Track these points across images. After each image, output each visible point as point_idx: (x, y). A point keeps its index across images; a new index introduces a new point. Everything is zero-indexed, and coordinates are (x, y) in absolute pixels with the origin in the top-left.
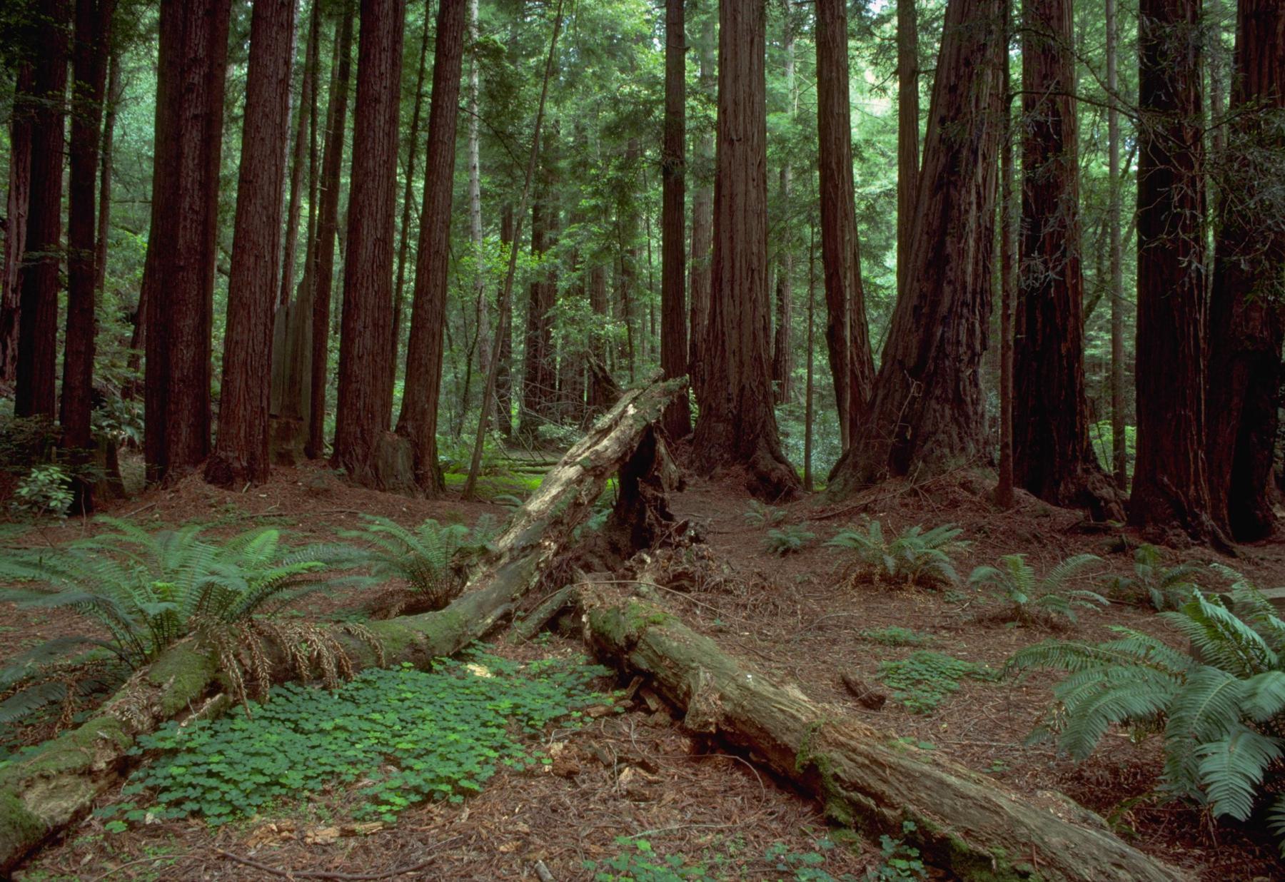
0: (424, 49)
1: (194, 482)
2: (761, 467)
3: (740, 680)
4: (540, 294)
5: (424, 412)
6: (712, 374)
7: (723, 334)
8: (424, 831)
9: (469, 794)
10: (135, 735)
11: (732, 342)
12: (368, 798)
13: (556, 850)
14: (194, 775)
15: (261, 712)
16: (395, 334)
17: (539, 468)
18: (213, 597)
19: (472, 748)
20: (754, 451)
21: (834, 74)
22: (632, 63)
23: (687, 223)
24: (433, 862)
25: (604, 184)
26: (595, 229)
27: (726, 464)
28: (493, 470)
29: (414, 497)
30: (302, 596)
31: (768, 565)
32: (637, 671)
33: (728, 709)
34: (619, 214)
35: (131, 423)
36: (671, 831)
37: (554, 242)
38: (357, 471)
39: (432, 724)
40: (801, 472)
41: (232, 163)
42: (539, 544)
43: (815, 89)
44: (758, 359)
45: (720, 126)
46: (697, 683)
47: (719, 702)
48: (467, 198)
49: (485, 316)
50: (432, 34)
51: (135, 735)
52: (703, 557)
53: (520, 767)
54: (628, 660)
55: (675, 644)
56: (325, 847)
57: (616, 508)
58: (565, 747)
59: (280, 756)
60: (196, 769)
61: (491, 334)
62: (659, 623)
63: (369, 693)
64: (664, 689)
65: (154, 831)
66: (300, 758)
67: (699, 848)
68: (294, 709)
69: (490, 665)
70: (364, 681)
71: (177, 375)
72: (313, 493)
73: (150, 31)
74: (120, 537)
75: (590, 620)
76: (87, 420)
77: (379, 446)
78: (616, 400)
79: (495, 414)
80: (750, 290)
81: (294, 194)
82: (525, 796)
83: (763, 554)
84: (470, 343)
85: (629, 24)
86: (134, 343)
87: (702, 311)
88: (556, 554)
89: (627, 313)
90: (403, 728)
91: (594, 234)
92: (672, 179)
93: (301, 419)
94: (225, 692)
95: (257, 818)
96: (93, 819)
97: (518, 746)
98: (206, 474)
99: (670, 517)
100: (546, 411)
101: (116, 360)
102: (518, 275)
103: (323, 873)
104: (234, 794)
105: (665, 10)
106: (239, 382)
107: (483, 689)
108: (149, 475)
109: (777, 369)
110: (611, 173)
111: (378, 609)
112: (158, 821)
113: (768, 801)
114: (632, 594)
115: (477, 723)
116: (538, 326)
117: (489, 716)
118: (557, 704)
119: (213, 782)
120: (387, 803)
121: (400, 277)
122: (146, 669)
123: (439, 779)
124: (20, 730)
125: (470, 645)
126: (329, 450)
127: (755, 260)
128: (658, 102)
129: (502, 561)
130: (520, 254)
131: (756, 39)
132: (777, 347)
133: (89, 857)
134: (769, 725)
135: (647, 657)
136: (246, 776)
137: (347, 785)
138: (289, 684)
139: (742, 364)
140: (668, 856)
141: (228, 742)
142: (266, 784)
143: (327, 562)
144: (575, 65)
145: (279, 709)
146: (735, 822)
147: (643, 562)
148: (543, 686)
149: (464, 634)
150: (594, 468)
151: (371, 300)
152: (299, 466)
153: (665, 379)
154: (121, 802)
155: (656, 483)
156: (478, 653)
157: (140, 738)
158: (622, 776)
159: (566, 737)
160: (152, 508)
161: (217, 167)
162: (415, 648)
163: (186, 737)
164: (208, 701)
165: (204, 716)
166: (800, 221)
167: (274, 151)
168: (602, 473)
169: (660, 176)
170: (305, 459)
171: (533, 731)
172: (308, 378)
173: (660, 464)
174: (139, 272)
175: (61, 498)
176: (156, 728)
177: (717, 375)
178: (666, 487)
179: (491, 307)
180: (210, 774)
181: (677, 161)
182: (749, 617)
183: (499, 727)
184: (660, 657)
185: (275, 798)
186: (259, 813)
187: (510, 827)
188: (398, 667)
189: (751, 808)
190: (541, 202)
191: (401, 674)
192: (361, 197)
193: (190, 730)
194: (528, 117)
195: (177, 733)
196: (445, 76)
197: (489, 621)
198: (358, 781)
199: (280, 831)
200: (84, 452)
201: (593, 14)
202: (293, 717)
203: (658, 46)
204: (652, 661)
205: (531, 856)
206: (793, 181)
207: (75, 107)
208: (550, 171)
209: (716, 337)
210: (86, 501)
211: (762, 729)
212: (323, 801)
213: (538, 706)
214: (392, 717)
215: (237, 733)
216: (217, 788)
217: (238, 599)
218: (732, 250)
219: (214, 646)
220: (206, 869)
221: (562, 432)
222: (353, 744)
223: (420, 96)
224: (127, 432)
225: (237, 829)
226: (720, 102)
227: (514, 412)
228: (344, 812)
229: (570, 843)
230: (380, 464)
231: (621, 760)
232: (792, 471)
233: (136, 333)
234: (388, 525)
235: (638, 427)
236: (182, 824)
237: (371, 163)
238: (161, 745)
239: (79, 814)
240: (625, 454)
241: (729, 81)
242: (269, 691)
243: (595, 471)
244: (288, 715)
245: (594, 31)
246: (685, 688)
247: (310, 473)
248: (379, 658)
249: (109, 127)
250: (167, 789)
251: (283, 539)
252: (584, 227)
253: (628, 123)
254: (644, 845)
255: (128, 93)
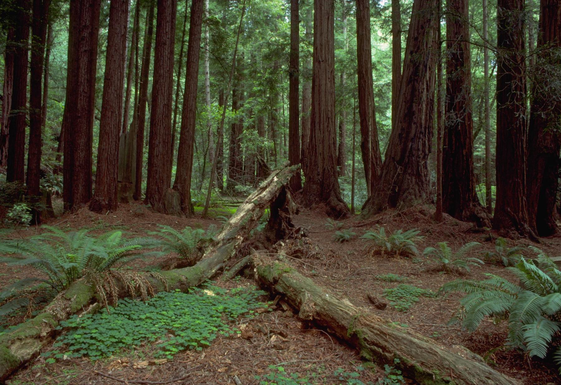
0: (185, 21)
1: (85, 210)
2: (332, 204)
3: (323, 297)
4: (236, 128)
5: (185, 180)
6: (311, 163)
7: (316, 146)
8: (185, 363)
9: (205, 347)
10: (59, 321)
11: (320, 149)
12: (160, 348)
13: (243, 371)
14: (85, 338)
15: (114, 311)
16: (172, 146)
17: (235, 204)
18: (93, 261)
19: (206, 327)
20: (329, 197)
21: (364, 32)
22: (276, 27)
23: (300, 97)
24: (189, 376)
25: (264, 80)
26: (260, 100)
27: (317, 203)
28: (215, 205)
29: (181, 217)
30: (132, 260)
31: (335, 247)
32: (278, 293)
33: (318, 309)
34: (270, 93)
35: (57, 185)
36: (293, 363)
37: (242, 105)
38: (156, 205)
39: (189, 316)
40: (350, 206)
41: (101, 71)
42: (235, 238)
43: (356, 39)
44: (331, 157)
45: (315, 55)
46: (304, 298)
47: (314, 307)
48: (204, 86)
49: (212, 138)
50: (189, 15)
51: (59, 321)
52: (307, 243)
53: (227, 335)
54: (274, 288)
55: (295, 281)
56: (142, 370)
57: (269, 222)
58: (247, 326)
59: (122, 330)
60: (85, 336)
61: (214, 146)
62: (288, 272)
63: (161, 302)
64: (290, 301)
65: (67, 363)
66: (131, 331)
67: (305, 370)
68: (129, 309)
69: (214, 290)
70: (159, 297)
71: (77, 163)
72: (137, 215)
73: (65, 14)
74: (52, 234)
75: (258, 271)
76: (38, 183)
77: (165, 195)
78: (269, 174)
79: (216, 181)
80: (328, 126)
81: (128, 85)
82: (229, 347)
83: (333, 242)
84: (205, 150)
85: (275, 10)
86: (58, 150)
87: (307, 136)
88: (243, 242)
89: (274, 137)
90: (176, 318)
91: (259, 102)
92: (293, 78)
93: (131, 183)
94: (98, 302)
95: (112, 357)
96: (41, 357)
97: (226, 326)
98: (90, 207)
99: (292, 226)
100: (238, 180)
101: (51, 157)
102: (226, 120)
103: (141, 381)
104: (102, 347)
105: (290, 5)
106: (104, 167)
107: (211, 301)
108: (65, 207)
109: (339, 161)
110: (267, 75)
111: (165, 266)
112: (69, 358)
113: (335, 350)
114: (276, 259)
115: (208, 316)
116: (235, 142)
117: (213, 313)
118: (243, 307)
119: (93, 341)
120: (169, 350)
121: (175, 121)
122: (64, 292)
123: (192, 340)
124: (9, 319)
125: (205, 282)
126: (144, 197)
127: (330, 113)
128: (287, 44)
129: (219, 245)
130: (227, 111)
131: (330, 17)
132: (339, 152)
133: (39, 374)
134: (336, 316)
135: (282, 287)
136: (108, 339)
137: (151, 343)
138: (126, 299)
139: (324, 159)
140: (292, 374)
141: (100, 324)
142: (116, 342)
143: (143, 245)
144: (251, 28)
145: (122, 309)
146: (321, 359)
147: (281, 245)
148: (237, 299)
149: (203, 277)
150: (259, 204)
151: (162, 131)
152: (131, 203)
153: (290, 165)
154: (53, 350)
155: (286, 211)
156: (209, 285)
157: (61, 322)
158: (272, 339)
159: (247, 322)
160: (66, 222)
161: (95, 73)
162: (181, 283)
163: (81, 322)
164: (91, 306)
165: (89, 313)
166: (349, 97)
167: (119, 66)
168: (263, 207)
169: (288, 77)
170: (133, 200)
171: (233, 319)
172: (134, 165)
173: (288, 203)
174: (61, 119)
175: (27, 218)
176: (68, 318)
177: (313, 164)
178: (291, 212)
179: (214, 134)
180: (92, 338)
181: (296, 70)
182: (327, 270)
183: (218, 317)
184: (288, 287)
185: (120, 348)
186: (113, 355)
187: (223, 361)
188: (174, 291)
189: (328, 353)
190: (236, 88)
191: (175, 294)
192: (157, 86)
193: (83, 319)
194: (231, 51)
195: (77, 320)
196: (194, 33)
197: (214, 271)
198: (156, 341)
199: (122, 363)
200: (36, 197)
201: (259, 6)
202: (128, 313)
203: (287, 20)
204: (285, 288)
205: (232, 374)
206: (346, 79)
207: (33, 47)
208: (240, 75)
209: (313, 147)
210: (38, 219)
211: (332, 318)
212: (141, 350)
213: (235, 308)
214: (171, 313)
215: (104, 320)
216: (95, 344)
217: (104, 262)
218: (320, 109)
219: (93, 282)
220: (90, 379)
221: (245, 189)
222: (154, 325)
223: (183, 42)
224: (56, 189)
225: (103, 362)
226: (314, 44)
227: (224, 180)
228: (150, 354)
229: (249, 368)
230: (166, 202)
231: (271, 332)
232: (346, 206)
233: (59, 145)
234: (169, 229)
235: (279, 186)
236: (79, 360)
237: (162, 71)
238: (70, 325)
239: (35, 355)
240: (273, 198)
241: (318, 35)
242: (117, 302)
243: (260, 205)
244: (126, 312)
245: (259, 14)
246: (299, 300)
247: (135, 207)
248: (165, 287)
249: (48, 55)
250: (73, 345)
251: (124, 235)
252: (255, 99)
253: (274, 54)
254: (281, 369)
255: (56, 41)
